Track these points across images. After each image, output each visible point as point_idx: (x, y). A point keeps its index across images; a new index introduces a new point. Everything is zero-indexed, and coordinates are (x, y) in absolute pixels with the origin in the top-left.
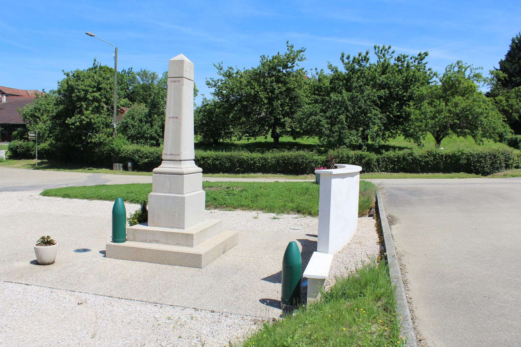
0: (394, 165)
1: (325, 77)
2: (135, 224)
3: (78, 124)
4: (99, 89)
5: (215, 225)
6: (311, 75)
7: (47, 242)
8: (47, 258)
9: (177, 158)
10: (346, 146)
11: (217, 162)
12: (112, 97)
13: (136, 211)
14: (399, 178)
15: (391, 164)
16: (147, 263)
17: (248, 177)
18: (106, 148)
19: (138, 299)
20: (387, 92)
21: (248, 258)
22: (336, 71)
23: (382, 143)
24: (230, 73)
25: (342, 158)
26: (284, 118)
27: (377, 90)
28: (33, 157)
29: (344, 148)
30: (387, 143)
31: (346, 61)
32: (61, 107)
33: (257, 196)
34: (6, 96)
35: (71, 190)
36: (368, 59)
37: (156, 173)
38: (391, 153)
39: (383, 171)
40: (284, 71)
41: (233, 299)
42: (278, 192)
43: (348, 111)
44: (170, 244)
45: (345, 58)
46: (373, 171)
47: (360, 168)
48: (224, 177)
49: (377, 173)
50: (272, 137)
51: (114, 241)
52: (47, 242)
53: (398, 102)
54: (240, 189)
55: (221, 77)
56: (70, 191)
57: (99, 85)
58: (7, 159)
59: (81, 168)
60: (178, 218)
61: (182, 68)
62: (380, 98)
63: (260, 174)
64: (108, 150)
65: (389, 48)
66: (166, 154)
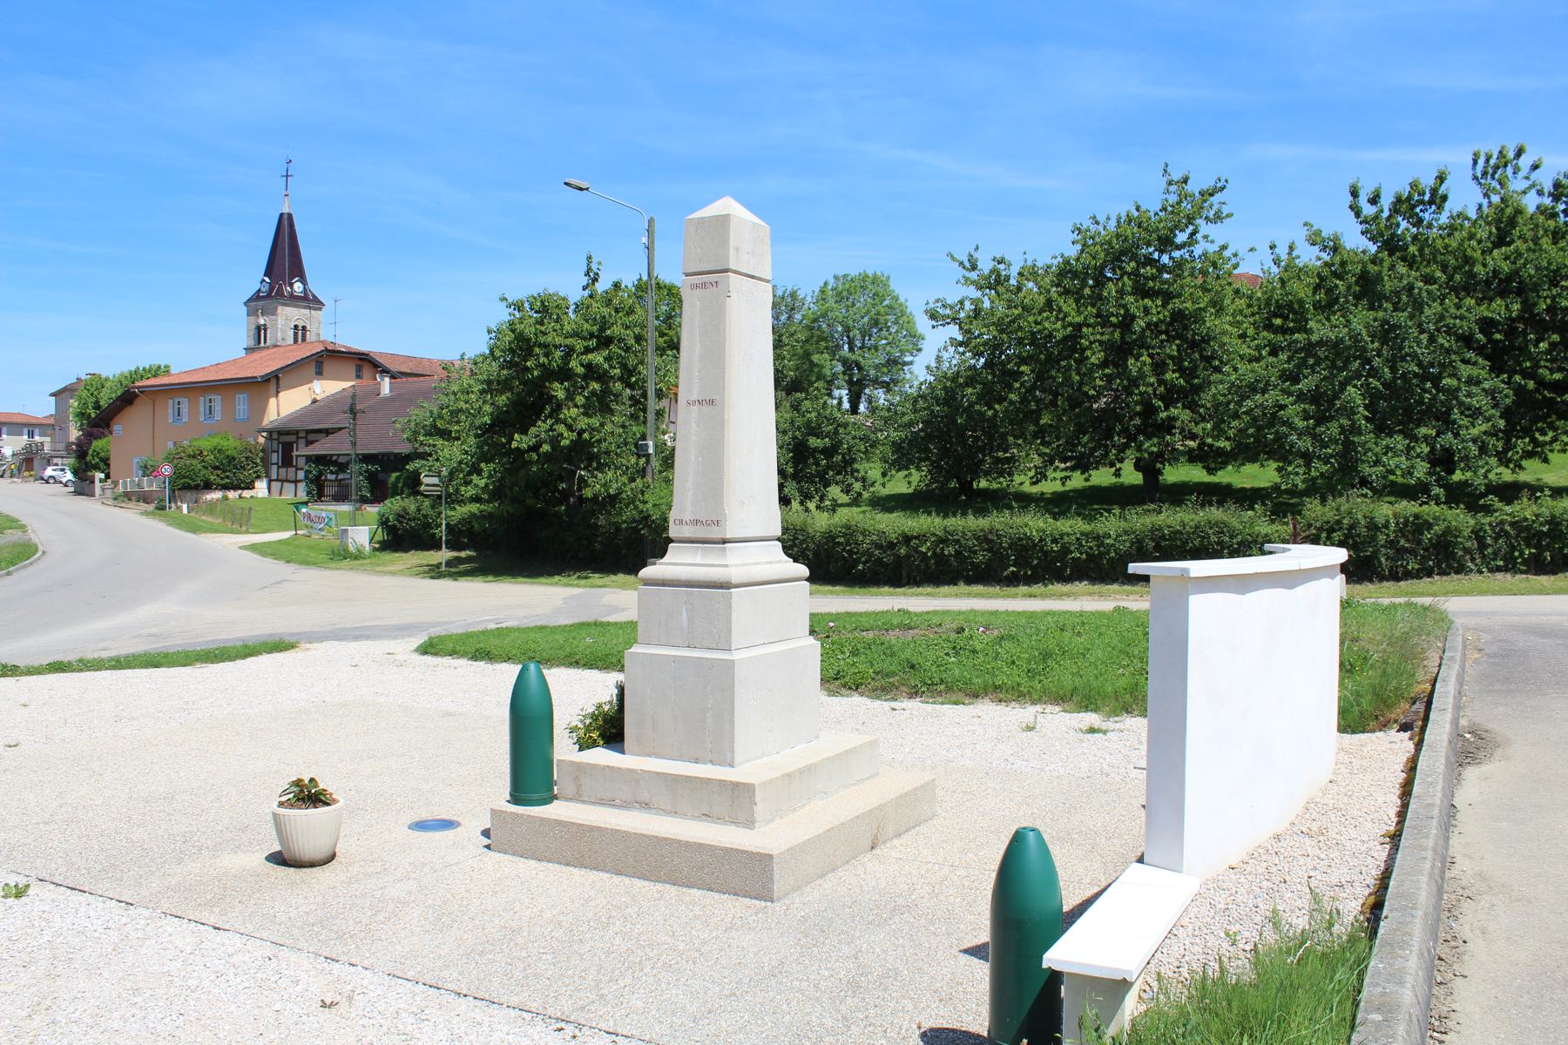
0: (1538, 546)
1: (1300, 273)
2: (594, 744)
3: (546, 448)
4: (605, 342)
5: (847, 753)
6: (1254, 265)
7: (309, 796)
8: (307, 846)
9: (715, 533)
10: (1373, 489)
11: (950, 550)
12: (642, 363)
13: (599, 706)
14: (1557, 592)
15: (1528, 546)
16: (605, 876)
17: (1043, 596)
18: (629, 513)
19: (515, 1000)
20: (1516, 307)
21: (946, 871)
22: (1335, 249)
23: (1507, 476)
24: (999, 275)
25: (1352, 527)
26: (1167, 408)
27: (1479, 302)
28: (435, 545)
29: (1365, 496)
30: (1523, 477)
31: (1369, 210)
32: (502, 400)
33: (1046, 656)
34: (393, 377)
35: (499, 636)
36: (1444, 198)
37: (649, 582)
38: (1524, 509)
39: (1499, 569)
40: (1165, 259)
41: (829, 1022)
42: (1115, 642)
43: (1374, 372)
44: (684, 816)
45: (1363, 201)
46: (1461, 569)
47: (1340, 555)
48: (969, 595)
49: (1475, 577)
50: (1137, 467)
51: (516, 799)
52: (309, 796)
53: (1556, 337)
54: (996, 633)
55: (973, 293)
56: (494, 641)
57: (602, 329)
58: (375, 549)
59: (551, 574)
60: (711, 730)
61: (723, 241)
62: (1487, 325)
63: (1082, 586)
64: (634, 521)
65: (1520, 152)
66: (681, 522)
